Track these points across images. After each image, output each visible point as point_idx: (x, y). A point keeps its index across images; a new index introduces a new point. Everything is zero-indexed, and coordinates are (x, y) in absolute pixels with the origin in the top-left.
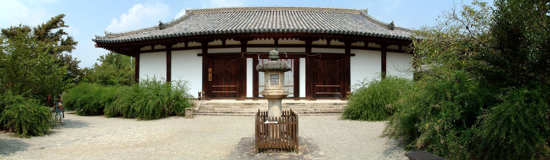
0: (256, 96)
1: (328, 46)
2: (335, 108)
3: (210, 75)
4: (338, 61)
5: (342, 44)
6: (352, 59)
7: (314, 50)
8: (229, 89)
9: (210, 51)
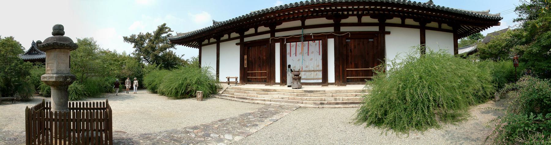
0: (284, 81)
1: (360, 24)
2: (352, 98)
3: (246, 62)
4: (372, 40)
5: (376, 21)
6: (387, 37)
7: (343, 29)
8: (261, 74)
9: (246, 40)
